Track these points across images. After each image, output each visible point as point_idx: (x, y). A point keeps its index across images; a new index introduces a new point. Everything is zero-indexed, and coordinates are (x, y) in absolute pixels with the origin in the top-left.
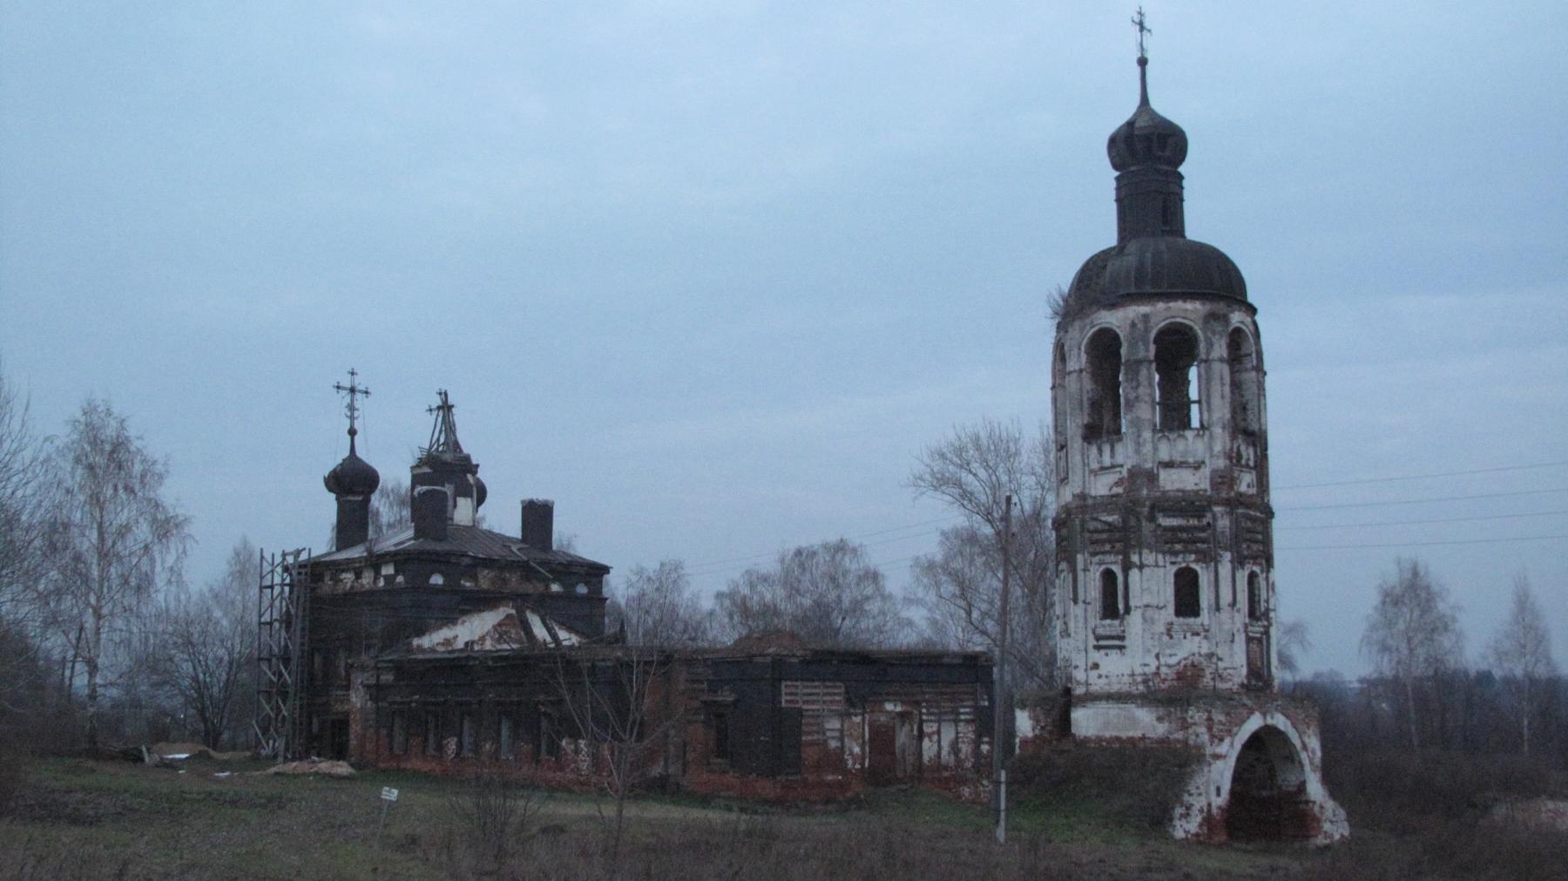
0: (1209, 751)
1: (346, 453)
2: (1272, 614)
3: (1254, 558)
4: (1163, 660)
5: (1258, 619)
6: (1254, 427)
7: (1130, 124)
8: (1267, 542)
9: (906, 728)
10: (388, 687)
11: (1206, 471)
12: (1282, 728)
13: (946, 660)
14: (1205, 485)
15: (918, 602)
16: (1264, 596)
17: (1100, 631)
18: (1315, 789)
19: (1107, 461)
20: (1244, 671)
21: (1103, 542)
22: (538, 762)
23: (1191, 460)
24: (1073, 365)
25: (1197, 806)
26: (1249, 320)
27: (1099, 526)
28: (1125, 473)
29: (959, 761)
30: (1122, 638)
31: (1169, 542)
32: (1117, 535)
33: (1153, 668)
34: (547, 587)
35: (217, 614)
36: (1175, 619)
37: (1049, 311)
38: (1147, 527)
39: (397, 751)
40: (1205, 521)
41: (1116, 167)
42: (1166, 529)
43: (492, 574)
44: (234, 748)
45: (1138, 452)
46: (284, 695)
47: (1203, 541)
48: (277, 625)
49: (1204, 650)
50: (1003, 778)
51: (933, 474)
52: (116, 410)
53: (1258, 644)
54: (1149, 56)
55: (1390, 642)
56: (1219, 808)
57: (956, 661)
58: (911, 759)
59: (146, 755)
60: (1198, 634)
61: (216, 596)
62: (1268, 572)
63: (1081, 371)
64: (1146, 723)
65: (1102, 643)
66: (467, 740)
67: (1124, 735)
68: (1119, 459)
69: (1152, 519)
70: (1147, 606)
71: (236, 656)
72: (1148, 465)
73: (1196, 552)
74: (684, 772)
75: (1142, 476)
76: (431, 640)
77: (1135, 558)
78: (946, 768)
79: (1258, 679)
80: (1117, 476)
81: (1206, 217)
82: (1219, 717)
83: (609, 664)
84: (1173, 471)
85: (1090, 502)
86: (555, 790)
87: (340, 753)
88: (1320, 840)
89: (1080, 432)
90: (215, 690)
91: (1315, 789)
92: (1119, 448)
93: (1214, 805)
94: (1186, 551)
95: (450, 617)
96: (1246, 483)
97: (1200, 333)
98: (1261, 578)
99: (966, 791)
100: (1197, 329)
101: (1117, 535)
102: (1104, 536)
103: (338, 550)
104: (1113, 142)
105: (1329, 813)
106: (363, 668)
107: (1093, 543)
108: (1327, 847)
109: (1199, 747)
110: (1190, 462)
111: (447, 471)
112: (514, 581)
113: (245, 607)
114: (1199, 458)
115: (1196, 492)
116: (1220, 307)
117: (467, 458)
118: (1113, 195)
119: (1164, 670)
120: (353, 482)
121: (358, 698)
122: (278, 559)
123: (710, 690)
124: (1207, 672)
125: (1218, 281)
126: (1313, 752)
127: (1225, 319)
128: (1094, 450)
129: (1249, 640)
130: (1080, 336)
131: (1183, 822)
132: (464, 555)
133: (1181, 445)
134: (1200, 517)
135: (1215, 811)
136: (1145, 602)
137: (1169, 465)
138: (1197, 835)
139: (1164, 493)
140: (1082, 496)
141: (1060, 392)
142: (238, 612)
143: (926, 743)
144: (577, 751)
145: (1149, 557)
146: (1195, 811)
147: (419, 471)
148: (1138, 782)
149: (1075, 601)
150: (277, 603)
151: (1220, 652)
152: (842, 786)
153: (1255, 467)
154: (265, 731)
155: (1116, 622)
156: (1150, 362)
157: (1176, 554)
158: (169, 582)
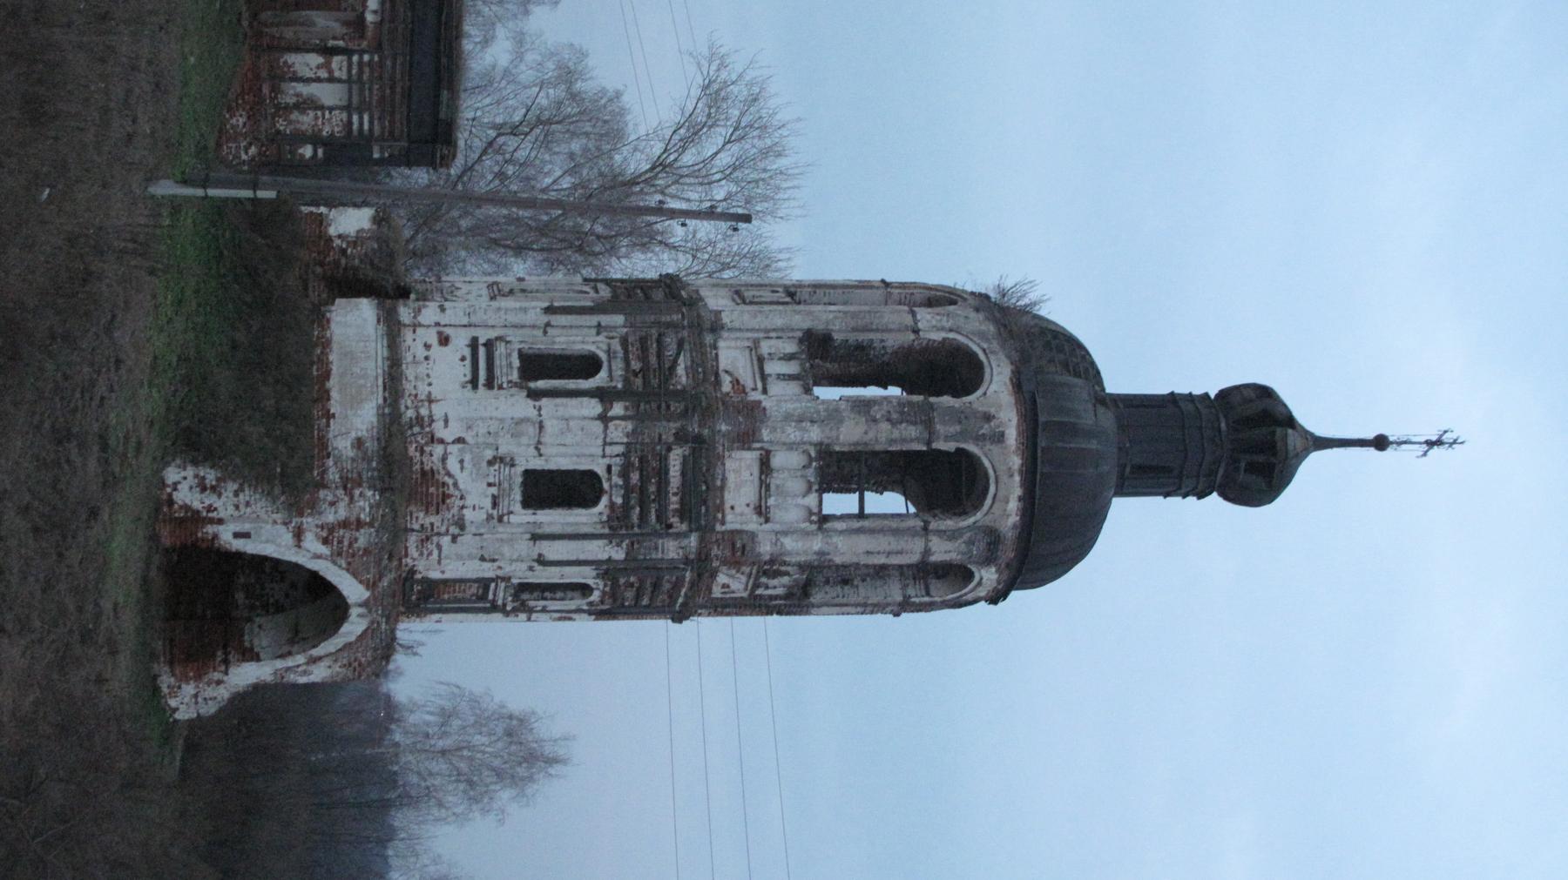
0: (309, 521)
2: (523, 616)
3: (614, 594)
4: (453, 449)
5: (516, 596)
6: (817, 597)
7: (1290, 421)
8: (637, 611)
9: (338, 28)
11: (752, 524)
12: (345, 628)
13: (445, 94)
14: (732, 522)
15: (519, 56)
16: (552, 605)
17: (500, 349)
18: (245, 675)
19: (772, 368)
20: (435, 575)
21: (644, 358)
23: (771, 501)
24: (926, 317)
25: (218, 504)
26: (982, 592)
27: (670, 352)
28: (755, 396)
29: (288, 109)
30: (490, 384)
31: (643, 464)
32: (655, 382)
33: (440, 431)
36: (519, 470)
37: (1008, 284)
38: (668, 430)
40: (674, 520)
41: (1224, 394)
42: (663, 460)
45: (788, 417)
47: (643, 517)
49: (468, 513)
50: (261, 194)
51: (725, 84)
53: (478, 598)
54: (1390, 452)
55: (456, 723)
56: (215, 536)
58: (289, 33)
60: (495, 505)
62: (590, 613)
63: (916, 331)
64: (354, 419)
65: (482, 351)
67: (333, 384)
68: (776, 388)
69: (681, 437)
70: (541, 427)
72: (765, 434)
73: (626, 506)
75: (749, 422)
77: (618, 409)
78: (275, 90)
79: (426, 597)
80: (749, 384)
81: (1145, 532)
82: (363, 538)
84: (756, 471)
85: (709, 339)
88: (166, 681)
89: (820, 326)
91: (245, 675)
92: (794, 388)
93: (221, 528)
94: (628, 489)
96: (730, 582)
97: (971, 520)
98: (582, 603)
99: (240, 120)
100: (977, 517)
101: (655, 382)
102: (653, 360)
104: (1265, 393)
105: (210, 692)
107: (643, 342)
108: (156, 690)
109: (313, 506)
110: (768, 498)
114: (776, 514)
115: (720, 508)
116: (1008, 553)
118: (1182, 389)
119: (438, 450)
124: (433, 519)
125: (1048, 544)
126: (305, 673)
127: (988, 561)
128: (791, 347)
129: (484, 583)
130: (972, 332)
131: (191, 481)
133: (797, 485)
134: (683, 513)
135: (210, 529)
136: (548, 424)
137: (765, 465)
138: (171, 502)
139: (721, 458)
140: (717, 327)
141: (879, 294)
143: (315, 59)
145: (619, 431)
146: (210, 499)
148: (259, 410)
149: (550, 310)
151: (466, 539)
153: (752, 596)
155: (515, 376)
156: (929, 443)
157: (624, 474)
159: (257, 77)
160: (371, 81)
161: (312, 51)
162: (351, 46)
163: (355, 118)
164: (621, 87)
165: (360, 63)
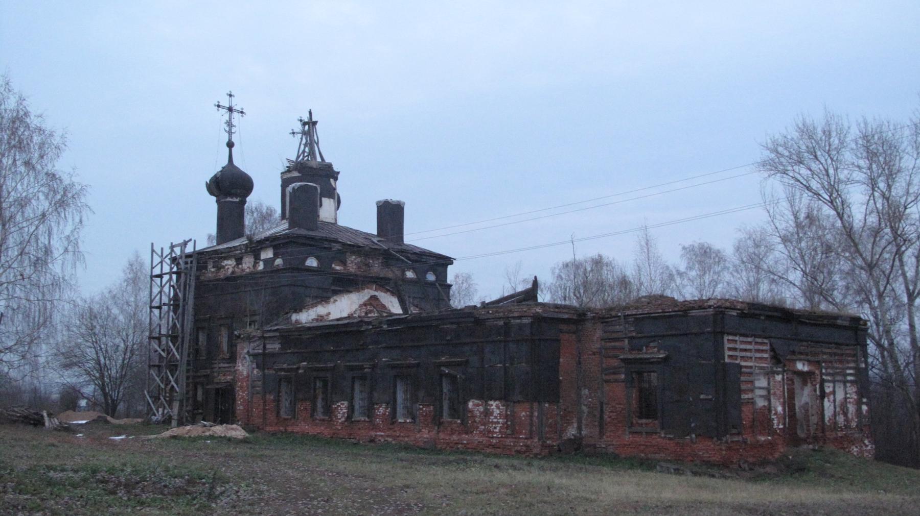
1: (225, 162)
9: (807, 390)
10: (273, 355)
13: (839, 322)
22: (440, 424)
34: (403, 272)
35: (115, 311)
39: (283, 414)
43: (359, 260)
44: (128, 417)
46: (173, 367)
48: (165, 308)
52: (15, 86)
57: (846, 323)
58: (814, 419)
59: (46, 419)
61: (114, 297)
66: (357, 404)
71: (130, 344)
74: (602, 433)
76: (306, 317)
83: (526, 321)
86: (464, 454)
87: (225, 416)
90: (114, 372)
95: (324, 298)
99: (855, 450)
103: (218, 244)
106: (249, 339)
111: (311, 180)
112: (376, 268)
113: (137, 306)
117: (330, 166)
120: (230, 187)
121: (244, 367)
122: (167, 251)
123: (632, 349)
132: (336, 241)
142: (130, 310)
143: (826, 403)
144: (487, 413)
147: (289, 175)
150: (166, 289)
152: (772, 445)
154: (156, 399)
158: (66, 250)
159: (836, 439)
160: (833, 368)
161: (823, 404)
162: (818, 380)
163: (849, 378)
164: (681, 247)
165: (827, 374)
